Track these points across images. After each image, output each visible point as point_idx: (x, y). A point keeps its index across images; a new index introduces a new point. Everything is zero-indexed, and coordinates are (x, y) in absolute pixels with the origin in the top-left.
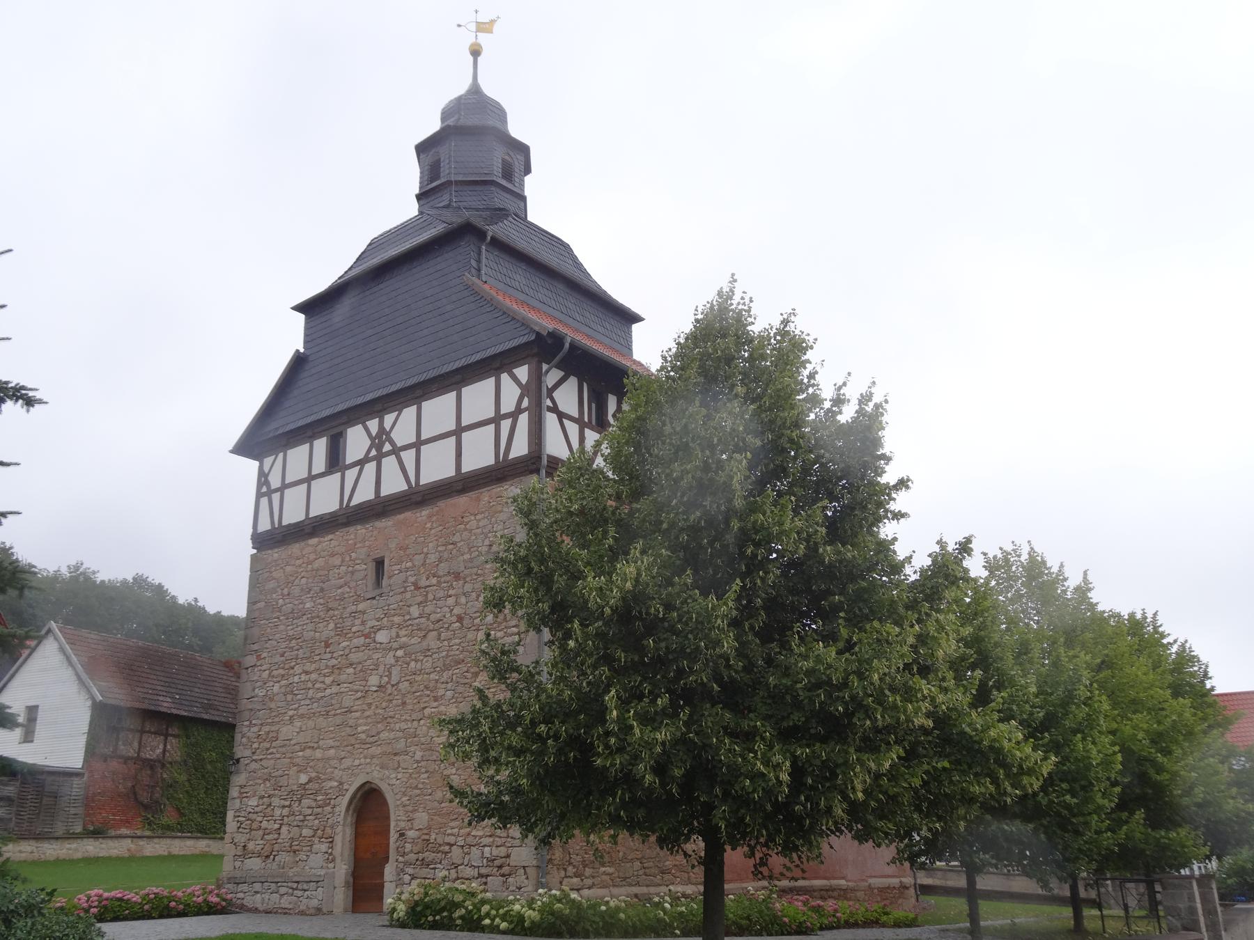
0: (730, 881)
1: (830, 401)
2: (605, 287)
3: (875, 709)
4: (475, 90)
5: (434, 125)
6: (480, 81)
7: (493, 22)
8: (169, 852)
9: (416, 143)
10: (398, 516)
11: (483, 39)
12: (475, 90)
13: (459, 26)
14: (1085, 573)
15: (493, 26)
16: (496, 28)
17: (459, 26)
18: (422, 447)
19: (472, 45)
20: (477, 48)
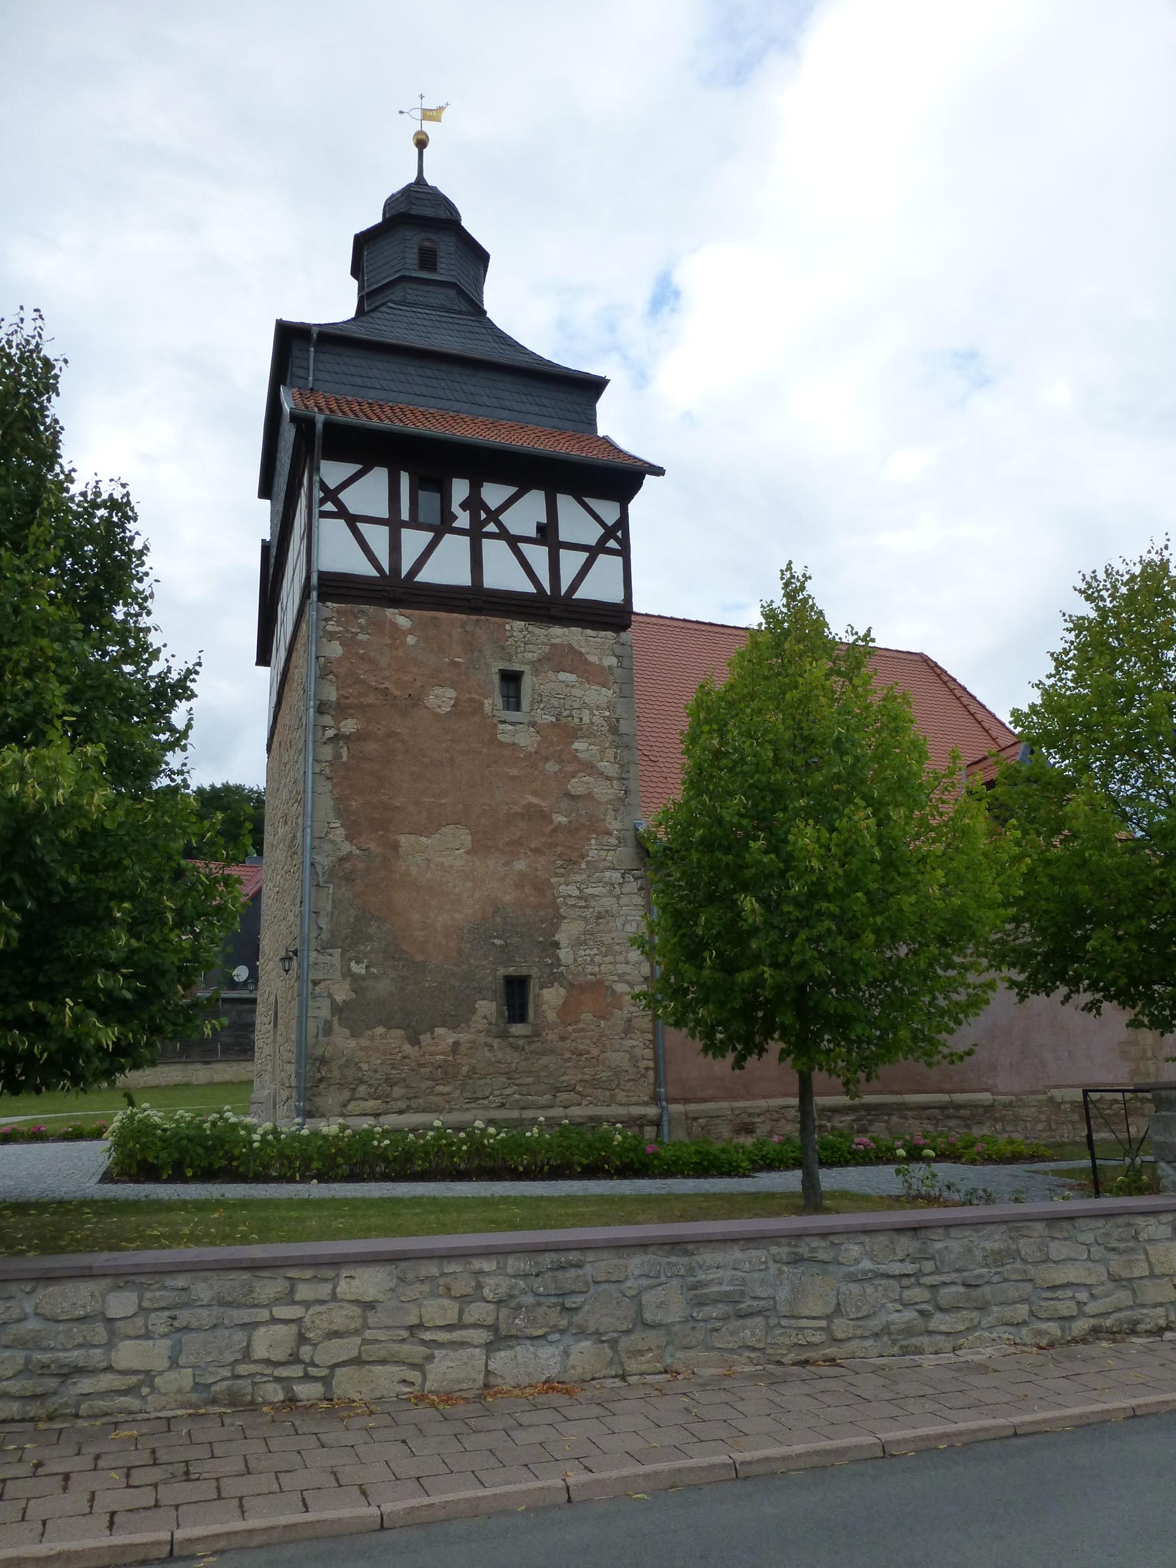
0: (821, 1094)
1: (930, 1167)
2: (547, 355)
3: (947, 1248)
4: (420, 180)
5: (374, 217)
6: (426, 175)
7: (441, 109)
8: (1156, 1325)
9: (358, 232)
10: (930, 1218)
11: (429, 127)
12: (420, 180)
13: (401, 112)
14: (1075, 589)
15: (441, 113)
16: (444, 115)
17: (401, 112)
18: (332, 488)
19: (417, 134)
20: (423, 137)
